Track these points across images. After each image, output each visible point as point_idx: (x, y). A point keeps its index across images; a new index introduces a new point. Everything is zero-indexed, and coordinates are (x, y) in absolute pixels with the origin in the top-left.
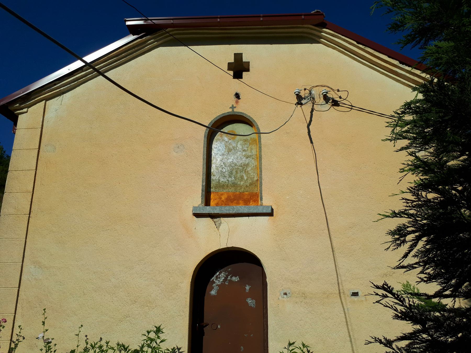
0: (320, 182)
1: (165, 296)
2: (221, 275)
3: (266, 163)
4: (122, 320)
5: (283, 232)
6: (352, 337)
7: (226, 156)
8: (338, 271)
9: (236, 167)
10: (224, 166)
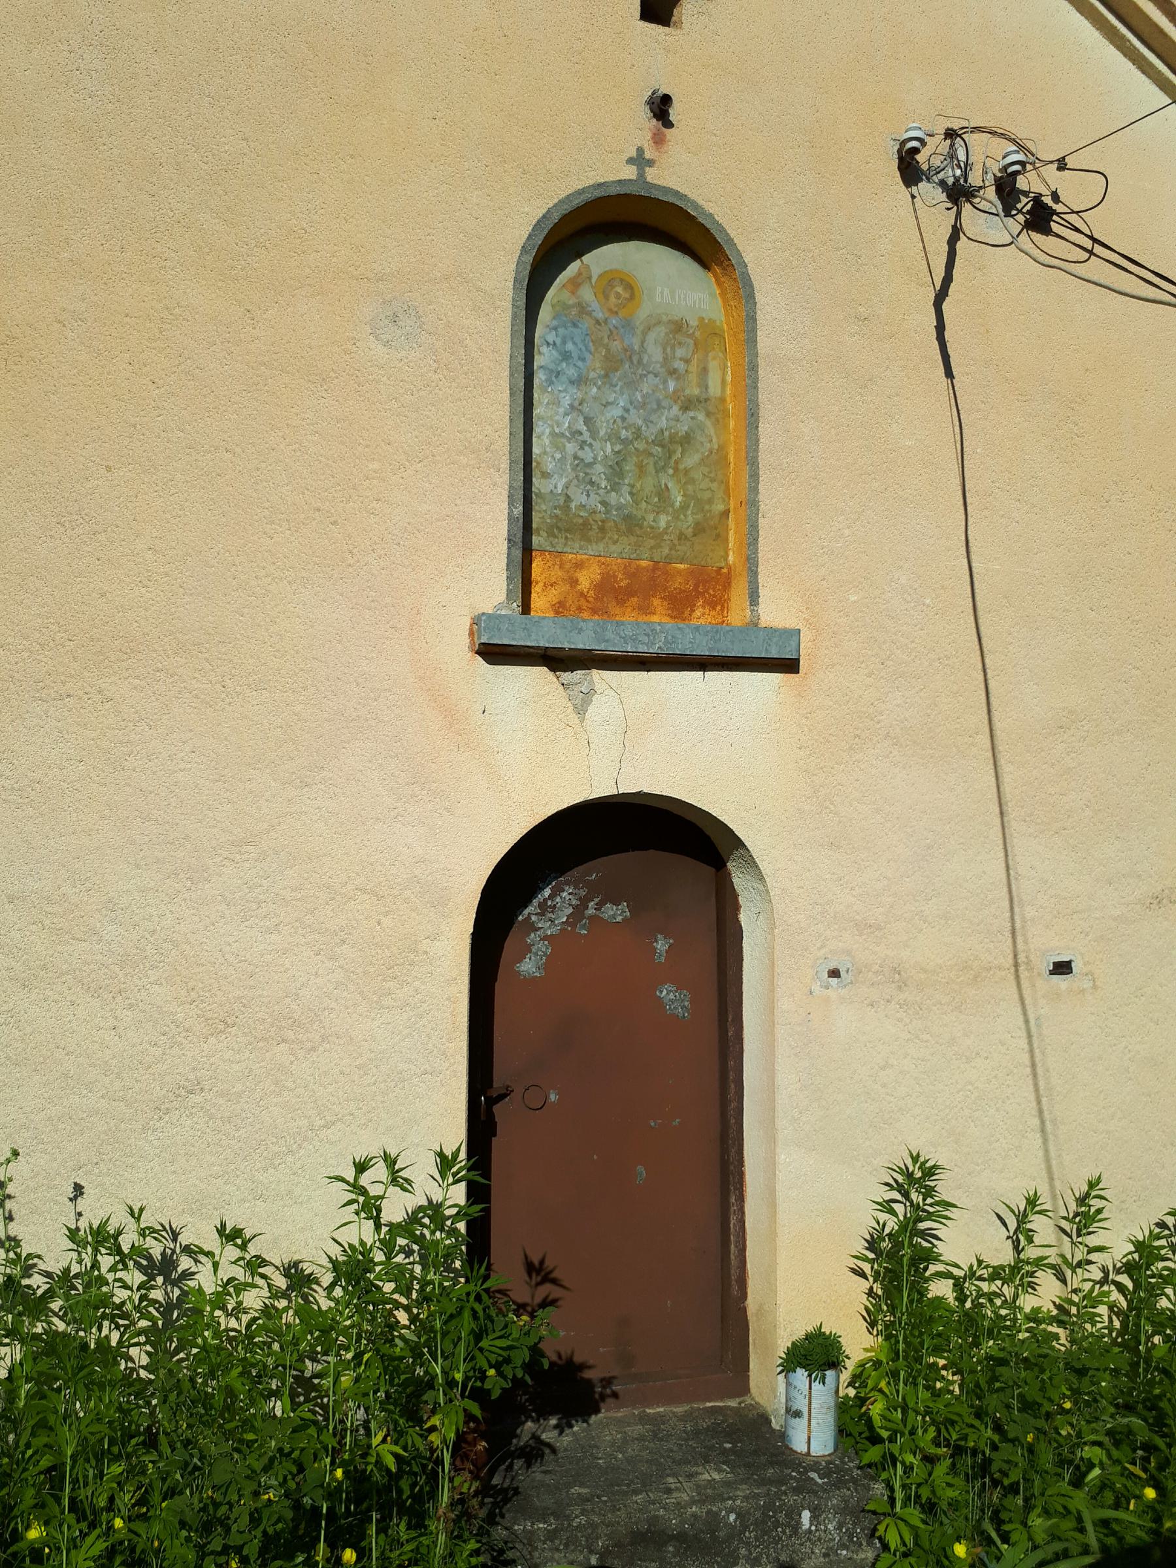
0: (970, 545)
1: (361, 993)
2: (558, 899)
3: (774, 440)
4: (167, 1106)
5: (832, 739)
6: (1046, 1115)
7: (595, 390)
8: (1014, 887)
9: (641, 445)
10: (586, 435)
